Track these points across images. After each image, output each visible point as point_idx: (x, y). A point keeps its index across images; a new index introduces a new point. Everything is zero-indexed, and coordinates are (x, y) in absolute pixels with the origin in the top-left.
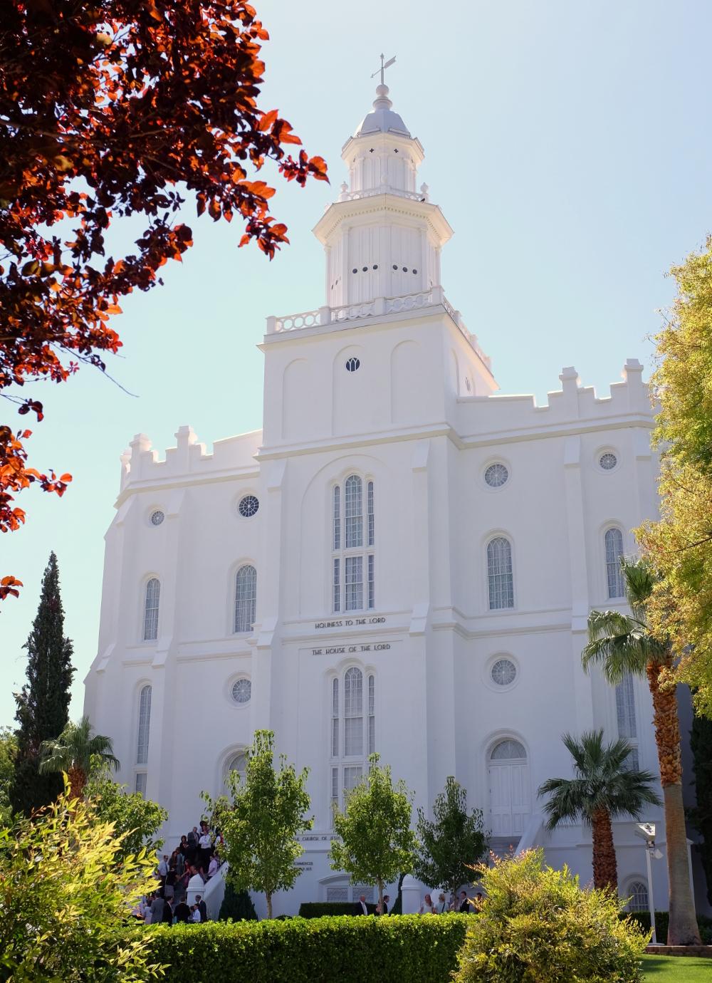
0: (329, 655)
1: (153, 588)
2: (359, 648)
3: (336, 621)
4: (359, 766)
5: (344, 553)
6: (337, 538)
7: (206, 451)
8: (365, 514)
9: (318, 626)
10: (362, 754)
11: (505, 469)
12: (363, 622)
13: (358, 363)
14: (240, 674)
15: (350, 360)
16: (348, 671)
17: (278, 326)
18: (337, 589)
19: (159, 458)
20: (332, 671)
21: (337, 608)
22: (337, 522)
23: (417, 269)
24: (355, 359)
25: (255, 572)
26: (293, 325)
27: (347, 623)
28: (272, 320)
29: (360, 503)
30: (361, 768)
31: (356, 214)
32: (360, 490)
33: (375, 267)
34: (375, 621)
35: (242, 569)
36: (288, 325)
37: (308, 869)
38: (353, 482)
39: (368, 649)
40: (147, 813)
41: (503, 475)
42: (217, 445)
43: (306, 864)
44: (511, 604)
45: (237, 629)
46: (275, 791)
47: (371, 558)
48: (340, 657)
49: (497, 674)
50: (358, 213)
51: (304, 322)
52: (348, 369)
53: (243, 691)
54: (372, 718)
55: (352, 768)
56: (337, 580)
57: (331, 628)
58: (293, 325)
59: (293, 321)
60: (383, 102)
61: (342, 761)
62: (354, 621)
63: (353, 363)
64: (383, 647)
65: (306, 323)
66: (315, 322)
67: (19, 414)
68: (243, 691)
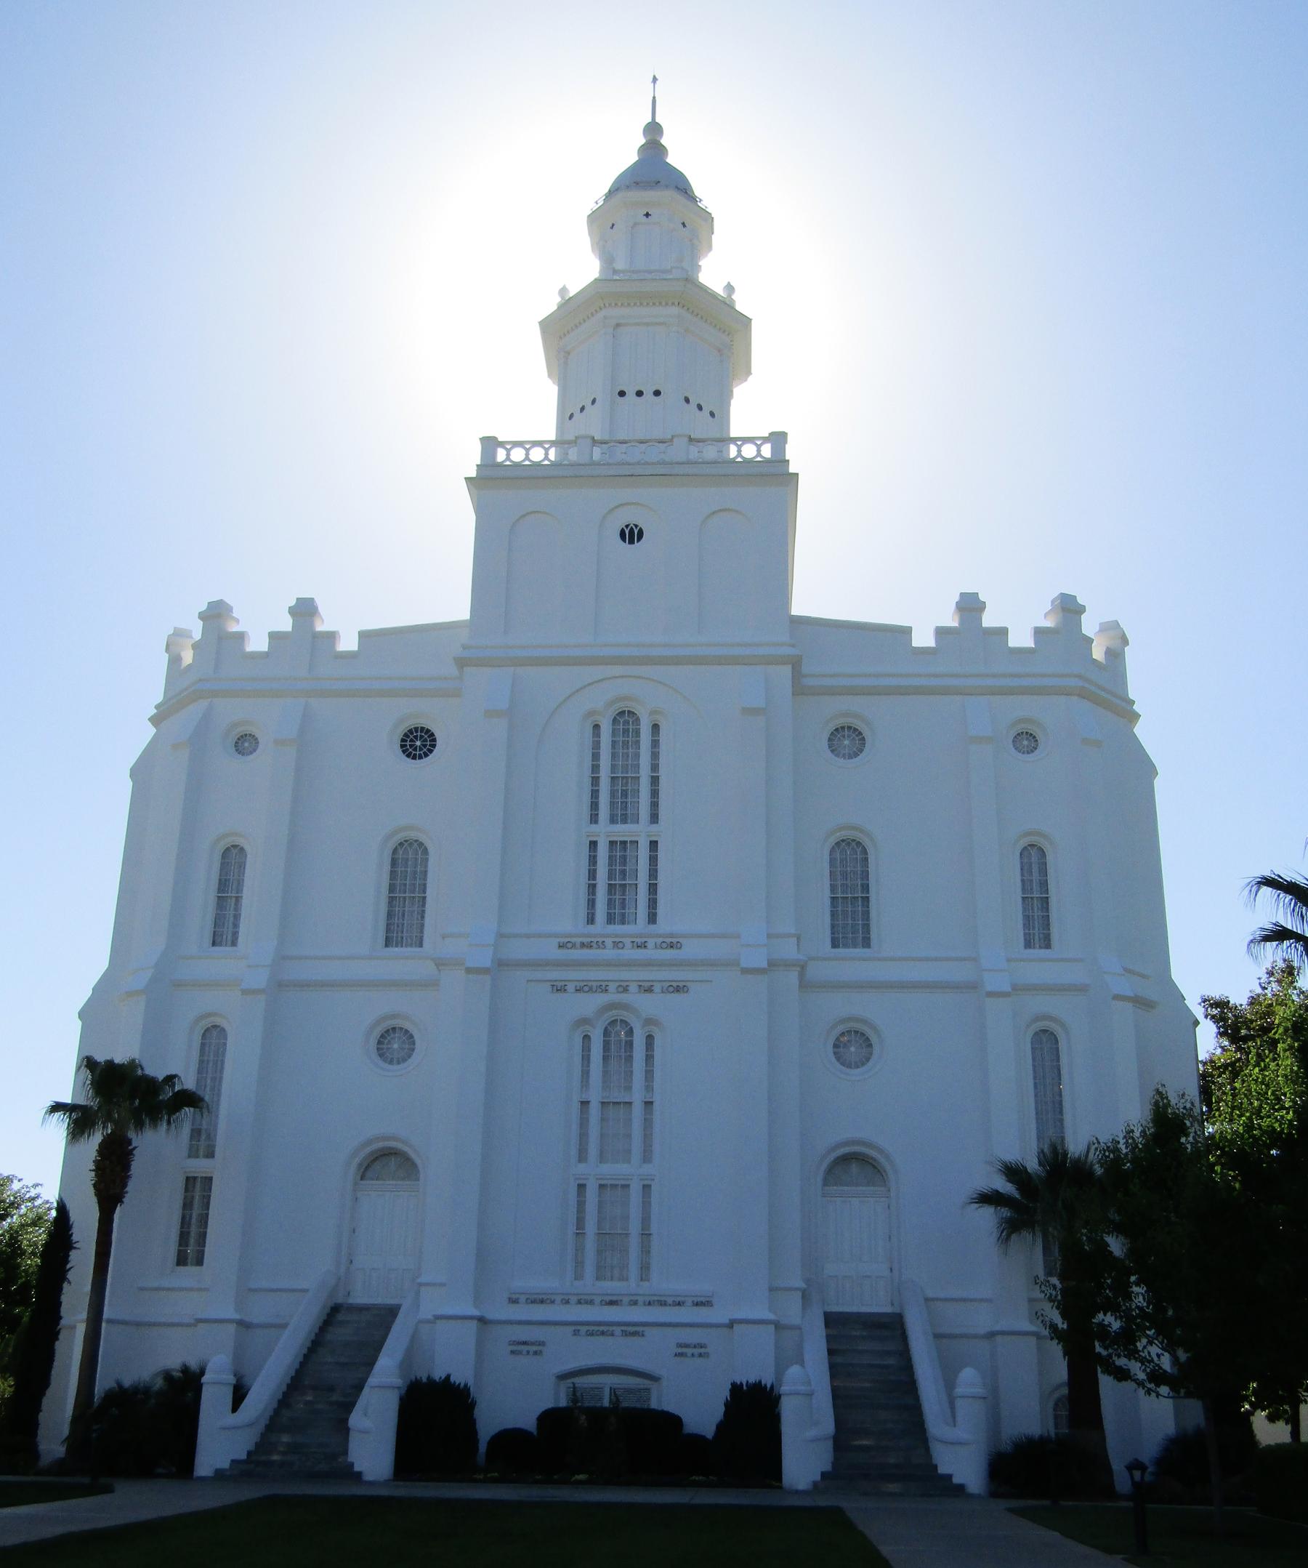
0: (579, 995)
4: (623, 1182)
6: (594, 806)
7: (348, 643)
9: (561, 946)
10: (629, 1162)
12: (643, 946)
14: (394, 1016)
16: (609, 1024)
17: (501, 455)
20: (584, 1021)
21: (591, 920)
22: (595, 781)
23: (654, 389)
24: (636, 526)
26: (527, 458)
27: (616, 944)
28: (490, 444)
29: (637, 756)
30: (628, 1186)
32: (637, 733)
35: (401, 844)
36: (518, 455)
38: (625, 720)
39: (649, 990)
41: (1033, 740)
43: (533, 1344)
44: (867, 943)
47: (654, 845)
48: (601, 999)
51: (527, 455)
53: (396, 1046)
54: (649, 1104)
55: (611, 1185)
56: (592, 874)
57: (586, 951)
58: (527, 458)
61: (594, 1171)
62: (627, 941)
63: (632, 531)
64: (678, 990)
65: (762, 453)
66: (546, 457)
68: (396, 1046)
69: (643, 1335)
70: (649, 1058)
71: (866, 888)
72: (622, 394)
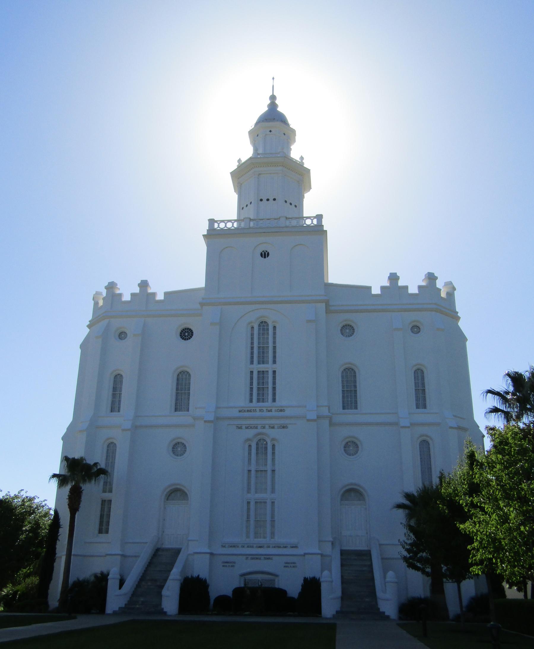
0: (247, 430)
1: (118, 380)
2: (267, 427)
3: (253, 409)
5: (257, 367)
6: (252, 358)
8: (271, 345)
11: (353, 327)
12: (271, 411)
13: (268, 254)
15: (263, 251)
18: (251, 389)
19: (127, 297)
20: (248, 440)
21: (251, 401)
24: (267, 251)
25: (190, 375)
26: (226, 226)
28: (212, 222)
31: (250, 170)
32: (268, 329)
33: (274, 200)
34: (278, 411)
37: (232, 566)
38: (263, 325)
39: (273, 428)
40: (509, 503)
42: (166, 294)
43: (231, 563)
44: (356, 408)
45: (176, 410)
46: (451, 498)
47: (274, 372)
49: (347, 449)
50: (279, 165)
51: (226, 225)
52: (262, 257)
54: (273, 471)
55: (260, 502)
56: (251, 384)
58: (226, 226)
59: (226, 224)
60: (273, 106)
63: (265, 253)
64: (284, 427)
65: (220, 226)
67: (322, 214)
68: (179, 449)
69: (272, 559)
70: (273, 453)
71: (355, 386)
72: (261, 200)
